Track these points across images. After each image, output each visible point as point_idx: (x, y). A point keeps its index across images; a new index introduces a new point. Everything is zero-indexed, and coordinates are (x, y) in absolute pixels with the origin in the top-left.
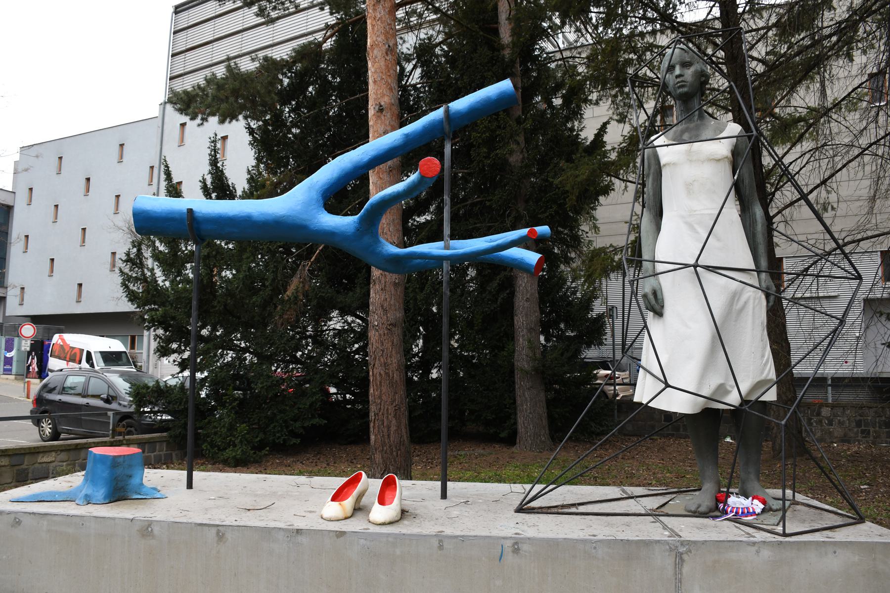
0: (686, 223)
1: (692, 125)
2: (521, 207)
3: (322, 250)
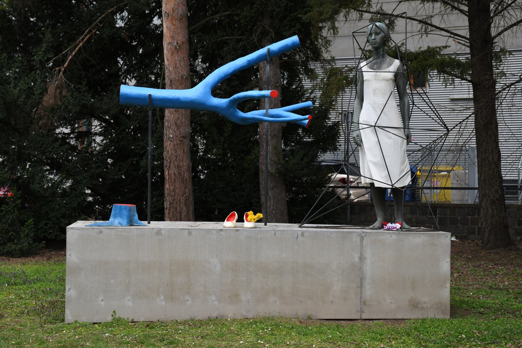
0: (372, 107)
1: (379, 61)
2: (267, 22)
3: (71, 59)
